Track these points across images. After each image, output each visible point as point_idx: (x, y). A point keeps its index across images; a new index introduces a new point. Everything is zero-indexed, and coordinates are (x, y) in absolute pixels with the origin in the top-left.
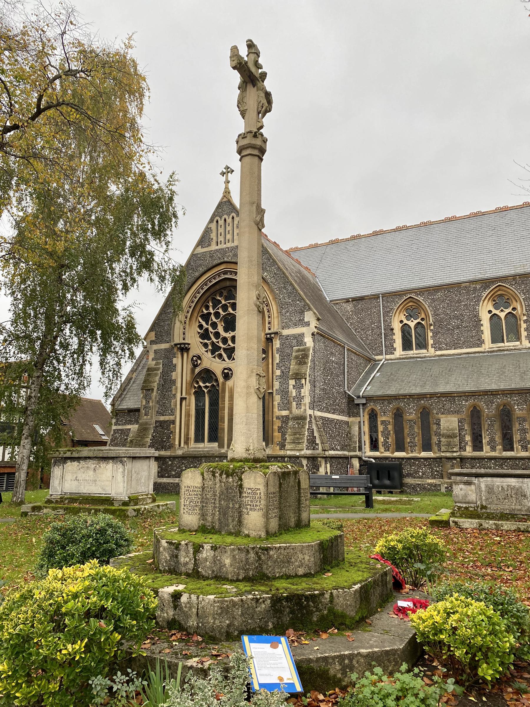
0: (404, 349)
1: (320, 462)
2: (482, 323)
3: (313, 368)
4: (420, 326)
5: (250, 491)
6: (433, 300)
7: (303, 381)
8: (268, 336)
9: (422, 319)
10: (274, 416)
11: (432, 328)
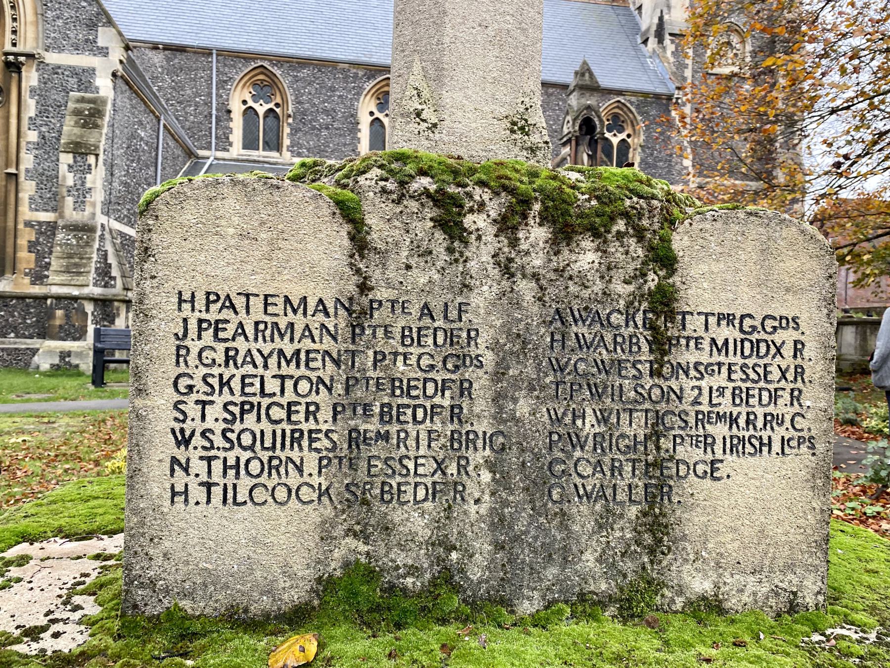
0: (245, 147)
1: (118, 309)
2: (359, 127)
3: (112, 139)
4: (271, 115)
5: (725, 332)
6: (296, 79)
7: (91, 159)
8: (11, 58)
9: (277, 105)
10: (21, 219)
11: (290, 120)
